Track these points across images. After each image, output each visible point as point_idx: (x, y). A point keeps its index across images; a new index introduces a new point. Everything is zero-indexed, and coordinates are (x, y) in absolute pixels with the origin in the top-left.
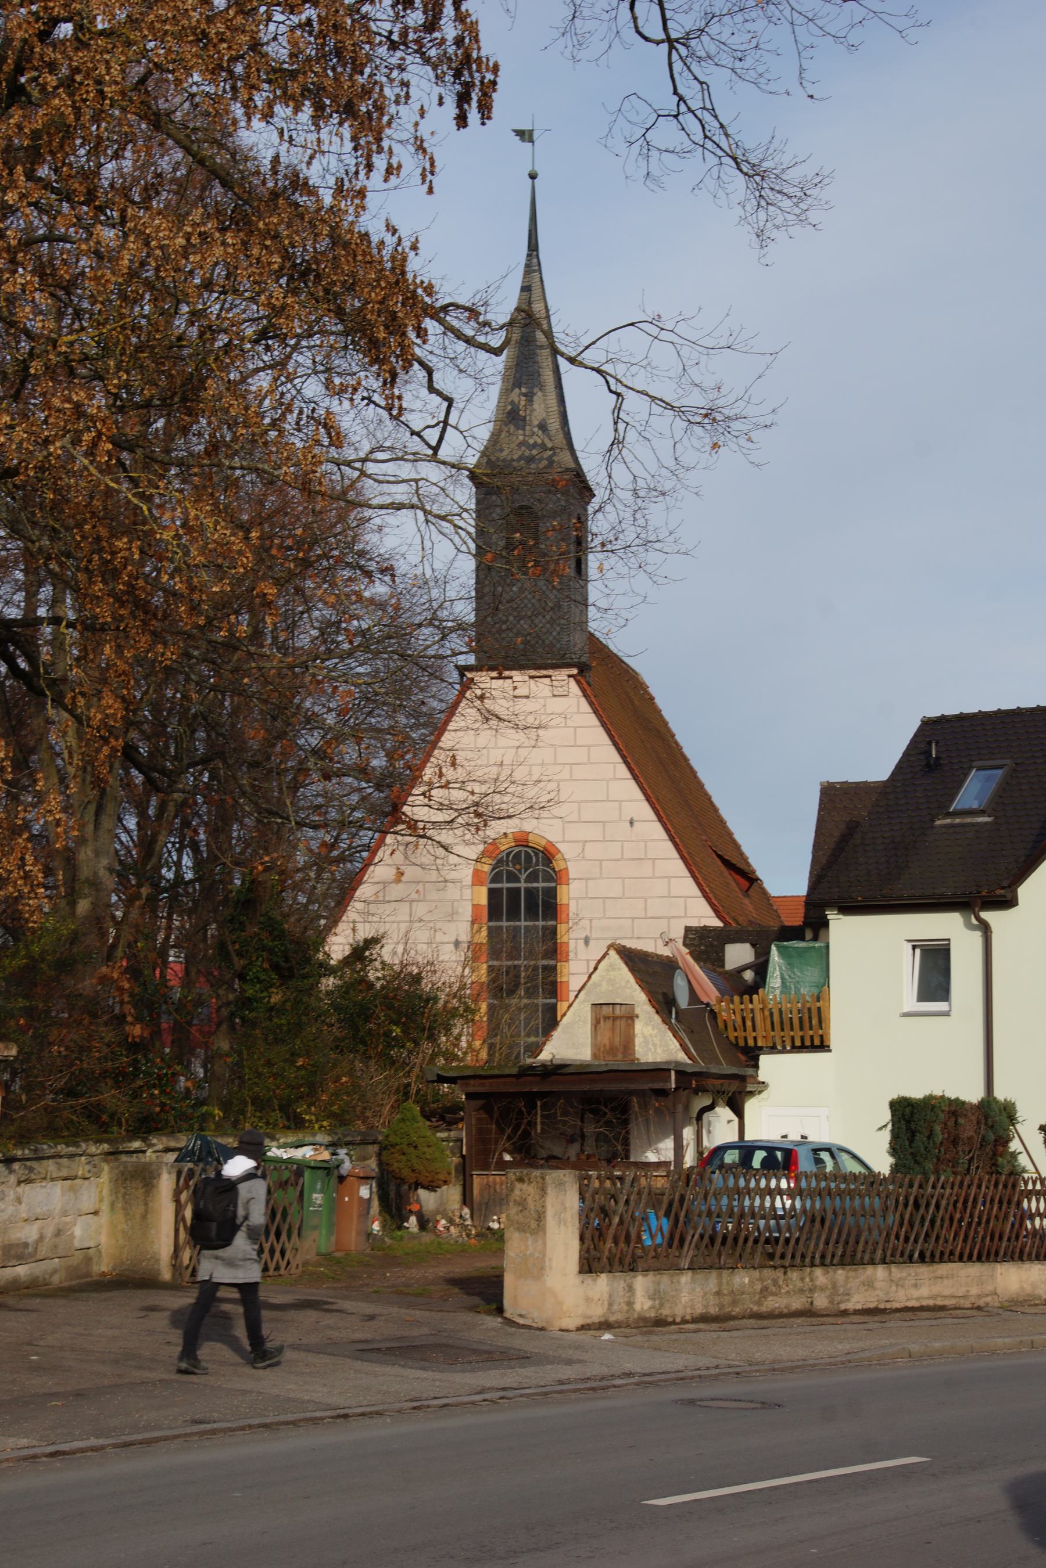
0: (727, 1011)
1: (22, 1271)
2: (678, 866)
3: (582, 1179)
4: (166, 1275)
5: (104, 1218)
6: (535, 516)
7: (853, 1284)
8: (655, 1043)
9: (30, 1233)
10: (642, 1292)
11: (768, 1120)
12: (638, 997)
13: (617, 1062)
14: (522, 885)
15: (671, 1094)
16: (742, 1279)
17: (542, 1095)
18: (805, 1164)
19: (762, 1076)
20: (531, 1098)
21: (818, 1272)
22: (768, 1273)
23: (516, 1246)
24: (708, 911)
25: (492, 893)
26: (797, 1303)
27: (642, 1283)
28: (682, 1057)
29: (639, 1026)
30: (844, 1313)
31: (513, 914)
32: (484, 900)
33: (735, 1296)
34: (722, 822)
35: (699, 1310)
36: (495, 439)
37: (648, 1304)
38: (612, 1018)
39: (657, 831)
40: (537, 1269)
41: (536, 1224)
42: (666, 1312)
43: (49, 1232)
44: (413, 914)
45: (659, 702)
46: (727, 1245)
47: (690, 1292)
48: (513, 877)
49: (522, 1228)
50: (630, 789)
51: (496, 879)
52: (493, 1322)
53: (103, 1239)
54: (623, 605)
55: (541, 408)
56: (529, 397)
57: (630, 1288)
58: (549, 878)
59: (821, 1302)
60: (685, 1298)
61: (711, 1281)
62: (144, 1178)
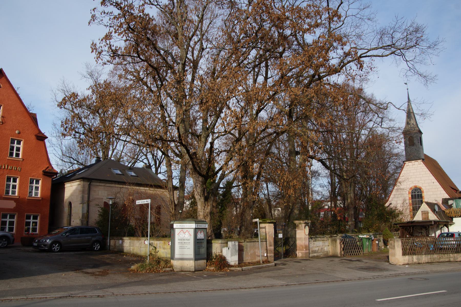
0: (447, 211)
1: (315, 254)
2: (442, 189)
3: (402, 240)
4: (339, 255)
5: (330, 247)
6: (413, 137)
7: (458, 256)
8: (432, 217)
9: (317, 249)
10: (415, 258)
11: (452, 229)
12: (429, 210)
13: (426, 220)
14: (417, 194)
15: (437, 225)
16: (435, 256)
17: (412, 226)
18: (456, 236)
19: (454, 221)
20: (410, 227)
21: (451, 254)
22: (440, 255)
23: (391, 251)
24: (448, 196)
25: (412, 195)
26: (447, 260)
27: (415, 257)
28: (437, 219)
29: (429, 214)
30: (457, 261)
31: (415, 198)
32: (410, 196)
33: (434, 259)
34: (452, 182)
35: (427, 261)
36: (406, 127)
37: (416, 260)
38: (425, 213)
39: (438, 184)
40: (394, 255)
41: (394, 248)
42: (420, 262)
43: (320, 249)
44: (398, 200)
45: (440, 164)
46: (440, 250)
47: (424, 258)
48: (415, 193)
49: (391, 248)
50: (433, 177)
51: (412, 193)
52: (387, 264)
53: (330, 250)
54: (428, 148)
55: (412, 122)
56: (410, 120)
57: (413, 258)
58: (421, 192)
59: (452, 260)
60: (424, 259)
61: (429, 256)
62: (335, 241)
